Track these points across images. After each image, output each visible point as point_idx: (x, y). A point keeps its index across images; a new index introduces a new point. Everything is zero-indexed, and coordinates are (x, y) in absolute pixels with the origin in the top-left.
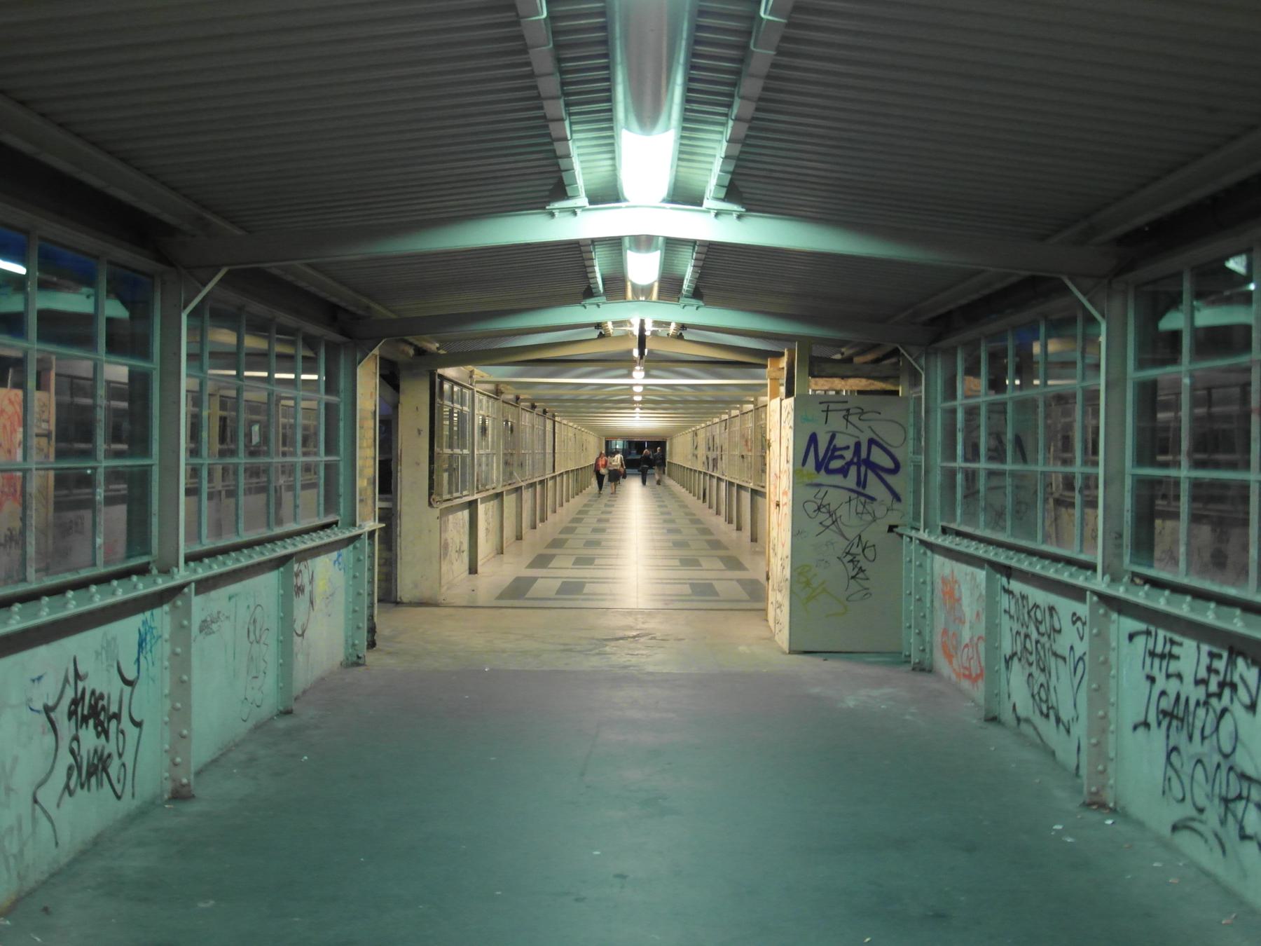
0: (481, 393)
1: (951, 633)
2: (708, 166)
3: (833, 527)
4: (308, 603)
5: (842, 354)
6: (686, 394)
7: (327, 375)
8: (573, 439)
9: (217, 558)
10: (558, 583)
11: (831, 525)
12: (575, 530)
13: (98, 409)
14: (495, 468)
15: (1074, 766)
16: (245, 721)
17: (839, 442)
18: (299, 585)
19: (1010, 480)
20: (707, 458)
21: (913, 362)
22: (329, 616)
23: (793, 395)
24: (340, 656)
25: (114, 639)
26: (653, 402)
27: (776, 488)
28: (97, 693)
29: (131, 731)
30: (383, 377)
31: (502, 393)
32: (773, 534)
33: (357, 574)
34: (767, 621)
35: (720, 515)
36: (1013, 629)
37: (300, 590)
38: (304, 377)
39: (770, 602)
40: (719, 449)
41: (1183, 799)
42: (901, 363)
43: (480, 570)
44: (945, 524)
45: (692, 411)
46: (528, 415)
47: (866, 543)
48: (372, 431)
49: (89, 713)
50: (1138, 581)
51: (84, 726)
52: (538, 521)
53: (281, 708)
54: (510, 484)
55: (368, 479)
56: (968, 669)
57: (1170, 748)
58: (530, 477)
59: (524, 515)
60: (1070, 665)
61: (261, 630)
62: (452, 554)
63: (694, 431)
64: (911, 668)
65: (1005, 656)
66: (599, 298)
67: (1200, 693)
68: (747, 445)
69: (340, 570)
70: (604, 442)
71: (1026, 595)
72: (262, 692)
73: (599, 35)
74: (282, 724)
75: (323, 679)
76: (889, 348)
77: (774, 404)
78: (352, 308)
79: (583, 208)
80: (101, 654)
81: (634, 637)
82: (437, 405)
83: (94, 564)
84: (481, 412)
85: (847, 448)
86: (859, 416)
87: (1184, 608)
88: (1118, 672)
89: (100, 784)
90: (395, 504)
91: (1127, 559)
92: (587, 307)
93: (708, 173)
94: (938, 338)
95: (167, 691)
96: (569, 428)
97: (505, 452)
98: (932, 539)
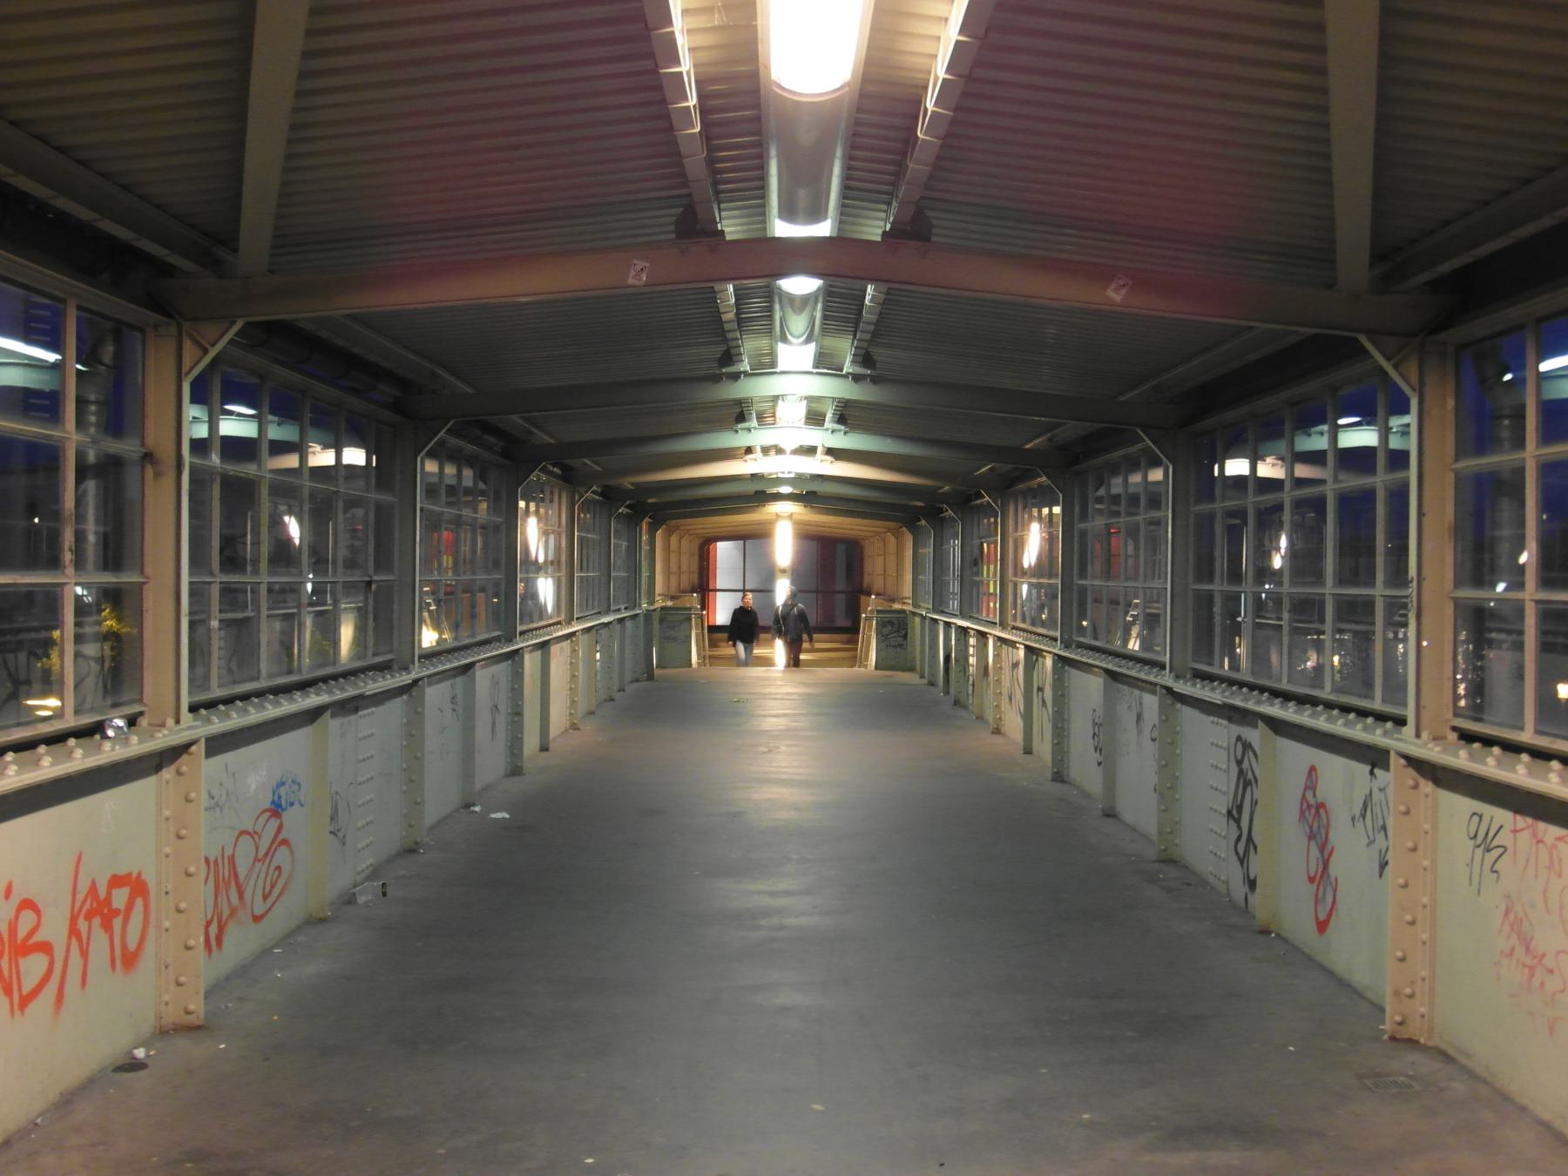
9: (218, 709)
73: (757, 183)
79: (755, 428)
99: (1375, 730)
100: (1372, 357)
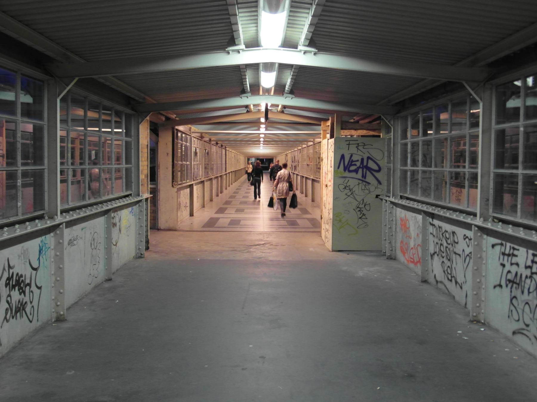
0: (195, 137)
1: (404, 243)
2: (301, 30)
3: (351, 196)
4: (118, 231)
5: (354, 119)
6: (281, 137)
7: (126, 129)
8: (234, 157)
10: (229, 220)
11: (351, 195)
12: (235, 197)
13: (18, 143)
14: (201, 170)
15: (464, 303)
16: (90, 284)
17: (355, 158)
18: (114, 223)
19: (433, 175)
20: (292, 166)
21: (388, 122)
22: (128, 236)
23: (334, 137)
24: (133, 254)
25: (27, 249)
26: (268, 142)
27: (325, 178)
28: (20, 274)
29: (36, 291)
30: (151, 130)
31: (204, 137)
32: (324, 199)
33: (141, 217)
34: (321, 237)
35: (298, 190)
36: (435, 241)
37: (115, 225)
38: (115, 130)
39: (322, 229)
40: (297, 162)
41: (518, 320)
42: (382, 123)
43: (194, 214)
44: (402, 194)
45: (285, 145)
46: (215, 147)
47: (366, 203)
48: (147, 154)
49: (15, 284)
50: (496, 220)
51: (13, 289)
52: (219, 193)
53: (107, 278)
54: (207, 177)
55: (145, 176)
56: (413, 259)
57: (512, 296)
58: (216, 174)
59: (213, 191)
60: (462, 258)
61: (97, 243)
62: (183, 208)
63: (286, 154)
64: (386, 258)
65: (431, 253)
66: (248, 94)
67: (528, 272)
68: (310, 160)
69: (133, 215)
70: (247, 159)
71: (441, 227)
72: (98, 271)
74: (107, 285)
75: (125, 264)
76: (377, 116)
77: (324, 142)
78: (137, 98)
79: (243, 50)
80: (21, 257)
81: (263, 244)
82: (175, 142)
83: (17, 215)
84: (195, 146)
85: (358, 161)
86: (363, 146)
87: (521, 233)
88: (486, 262)
89: (21, 316)
90: (157, 186)
91: (491, 210)
92: (242, 98)
93: (300, 33)
94: (399, 112)
95: (53, 272)
96: (232, 153)
97: (205, 163)
98: (396, 201)
99: (441, 212)
100: (467, 89)
